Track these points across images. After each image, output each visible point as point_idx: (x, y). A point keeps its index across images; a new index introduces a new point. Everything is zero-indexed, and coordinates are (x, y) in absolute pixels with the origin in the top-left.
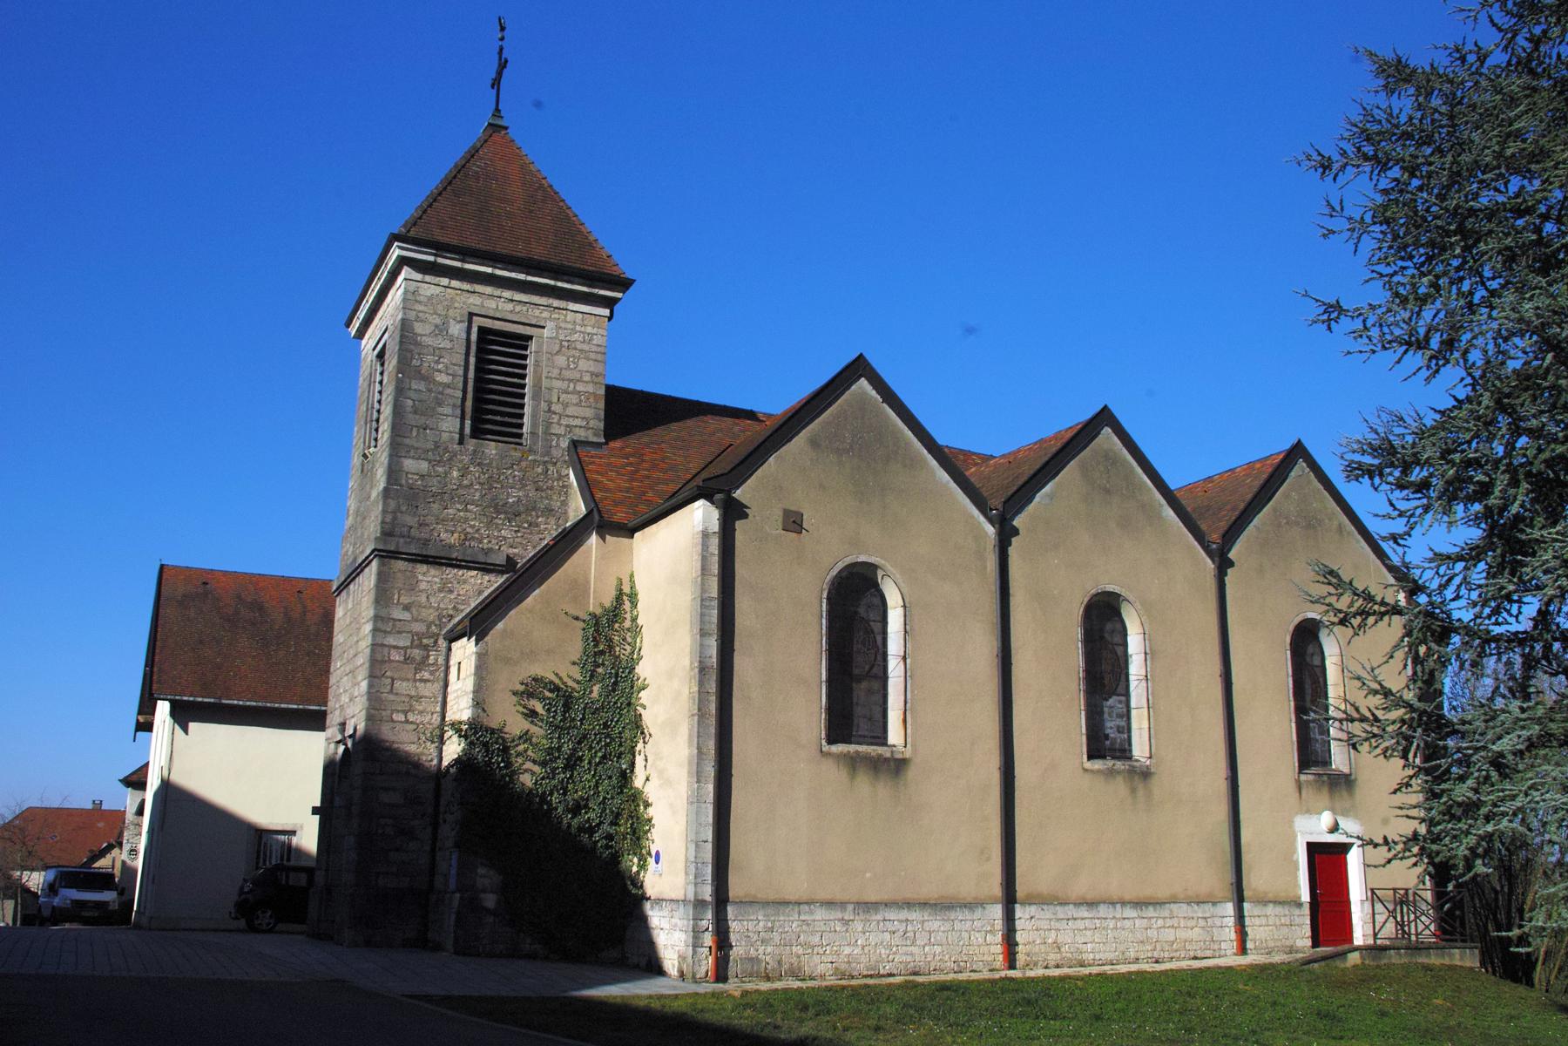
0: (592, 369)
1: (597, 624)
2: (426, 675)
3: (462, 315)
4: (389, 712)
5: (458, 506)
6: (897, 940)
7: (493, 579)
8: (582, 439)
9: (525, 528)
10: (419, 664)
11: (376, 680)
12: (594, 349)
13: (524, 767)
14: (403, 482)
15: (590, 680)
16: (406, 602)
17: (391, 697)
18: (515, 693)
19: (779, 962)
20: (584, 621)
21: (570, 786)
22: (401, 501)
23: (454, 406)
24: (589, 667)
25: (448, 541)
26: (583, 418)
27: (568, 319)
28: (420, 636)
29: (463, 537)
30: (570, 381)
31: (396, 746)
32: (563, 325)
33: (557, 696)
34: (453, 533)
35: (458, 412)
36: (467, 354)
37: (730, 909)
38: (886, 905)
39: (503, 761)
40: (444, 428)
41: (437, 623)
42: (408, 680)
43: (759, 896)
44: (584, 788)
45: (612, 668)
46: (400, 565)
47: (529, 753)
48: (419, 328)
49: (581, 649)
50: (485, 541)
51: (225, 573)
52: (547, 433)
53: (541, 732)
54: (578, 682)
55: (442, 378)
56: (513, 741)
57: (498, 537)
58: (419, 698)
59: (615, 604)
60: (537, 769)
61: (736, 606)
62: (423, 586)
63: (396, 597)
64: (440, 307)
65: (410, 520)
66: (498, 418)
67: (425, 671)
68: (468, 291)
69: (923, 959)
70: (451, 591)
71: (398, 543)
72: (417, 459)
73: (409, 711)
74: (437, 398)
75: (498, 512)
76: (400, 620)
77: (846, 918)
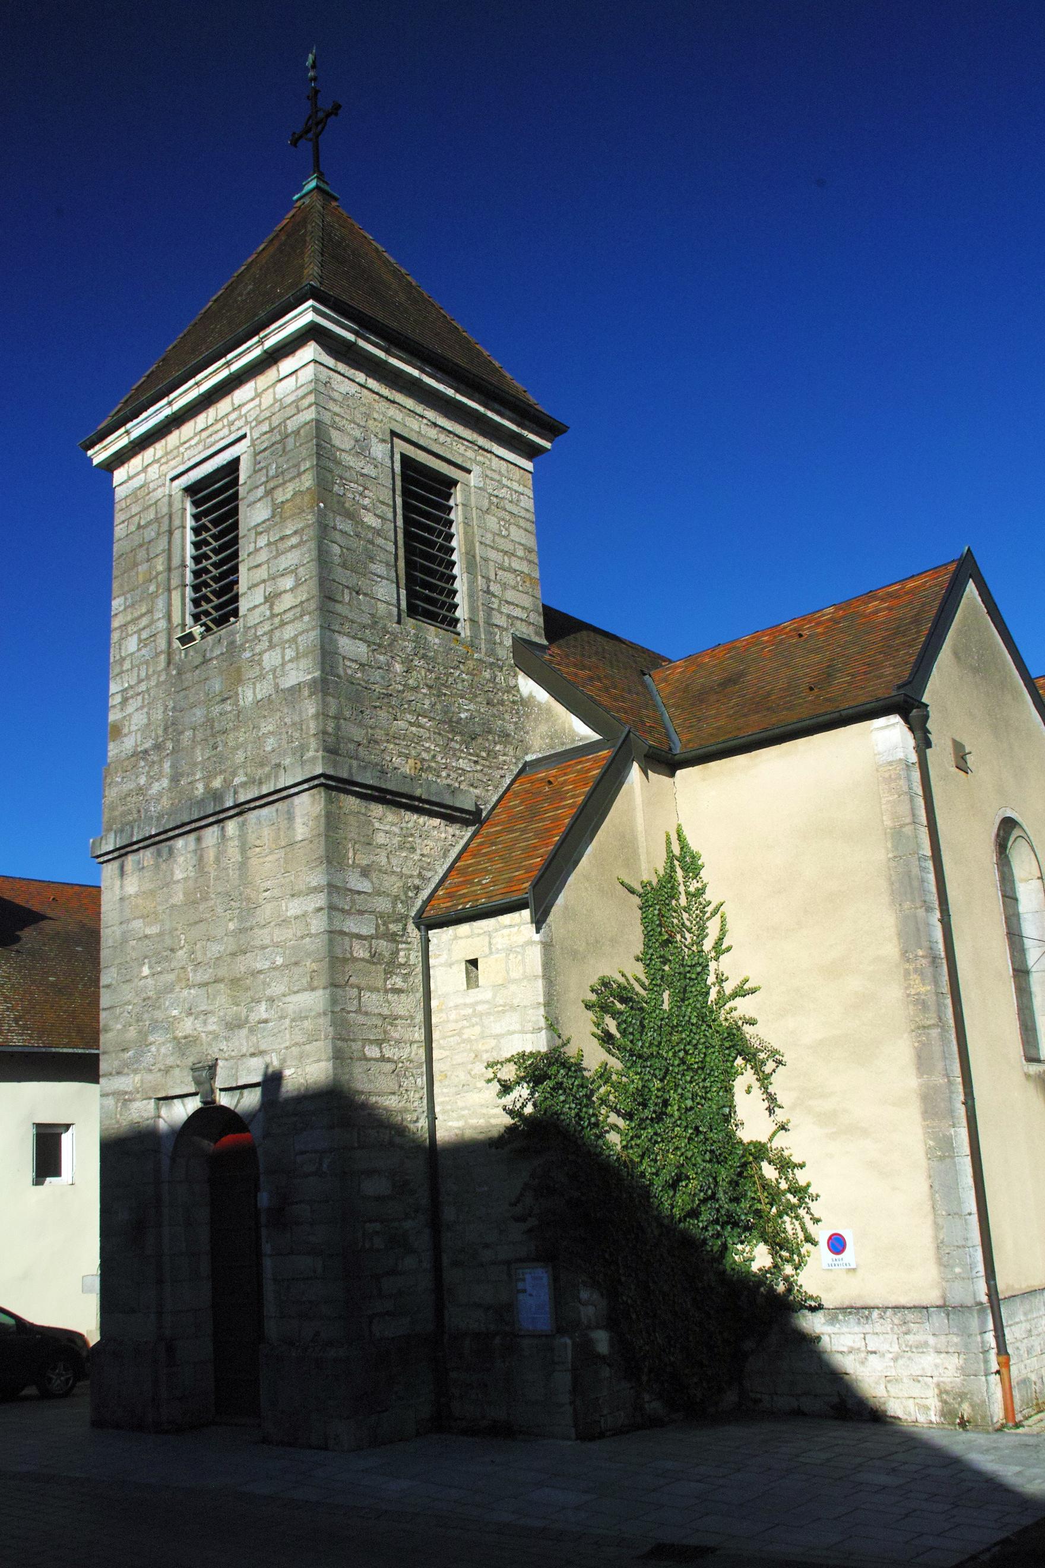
4: (360, 1043)
5: (409, 717)
7: (457, 832)
10: (388, 964)
11: (340, 991)
14: (341, 672)
16: (365, 862)
17: (361, 1019)
23: (388, 564)
26: (523, 608)
28: (384, 918)
29: (419, 766)
31: (373, 1099)
52: (489, 624)
63: (351, 854)
65: (358, 734)
68: (386, 398)
70: (413, 849)
71: (351, 767)
73: (384, 1041)
76: (359, 893)
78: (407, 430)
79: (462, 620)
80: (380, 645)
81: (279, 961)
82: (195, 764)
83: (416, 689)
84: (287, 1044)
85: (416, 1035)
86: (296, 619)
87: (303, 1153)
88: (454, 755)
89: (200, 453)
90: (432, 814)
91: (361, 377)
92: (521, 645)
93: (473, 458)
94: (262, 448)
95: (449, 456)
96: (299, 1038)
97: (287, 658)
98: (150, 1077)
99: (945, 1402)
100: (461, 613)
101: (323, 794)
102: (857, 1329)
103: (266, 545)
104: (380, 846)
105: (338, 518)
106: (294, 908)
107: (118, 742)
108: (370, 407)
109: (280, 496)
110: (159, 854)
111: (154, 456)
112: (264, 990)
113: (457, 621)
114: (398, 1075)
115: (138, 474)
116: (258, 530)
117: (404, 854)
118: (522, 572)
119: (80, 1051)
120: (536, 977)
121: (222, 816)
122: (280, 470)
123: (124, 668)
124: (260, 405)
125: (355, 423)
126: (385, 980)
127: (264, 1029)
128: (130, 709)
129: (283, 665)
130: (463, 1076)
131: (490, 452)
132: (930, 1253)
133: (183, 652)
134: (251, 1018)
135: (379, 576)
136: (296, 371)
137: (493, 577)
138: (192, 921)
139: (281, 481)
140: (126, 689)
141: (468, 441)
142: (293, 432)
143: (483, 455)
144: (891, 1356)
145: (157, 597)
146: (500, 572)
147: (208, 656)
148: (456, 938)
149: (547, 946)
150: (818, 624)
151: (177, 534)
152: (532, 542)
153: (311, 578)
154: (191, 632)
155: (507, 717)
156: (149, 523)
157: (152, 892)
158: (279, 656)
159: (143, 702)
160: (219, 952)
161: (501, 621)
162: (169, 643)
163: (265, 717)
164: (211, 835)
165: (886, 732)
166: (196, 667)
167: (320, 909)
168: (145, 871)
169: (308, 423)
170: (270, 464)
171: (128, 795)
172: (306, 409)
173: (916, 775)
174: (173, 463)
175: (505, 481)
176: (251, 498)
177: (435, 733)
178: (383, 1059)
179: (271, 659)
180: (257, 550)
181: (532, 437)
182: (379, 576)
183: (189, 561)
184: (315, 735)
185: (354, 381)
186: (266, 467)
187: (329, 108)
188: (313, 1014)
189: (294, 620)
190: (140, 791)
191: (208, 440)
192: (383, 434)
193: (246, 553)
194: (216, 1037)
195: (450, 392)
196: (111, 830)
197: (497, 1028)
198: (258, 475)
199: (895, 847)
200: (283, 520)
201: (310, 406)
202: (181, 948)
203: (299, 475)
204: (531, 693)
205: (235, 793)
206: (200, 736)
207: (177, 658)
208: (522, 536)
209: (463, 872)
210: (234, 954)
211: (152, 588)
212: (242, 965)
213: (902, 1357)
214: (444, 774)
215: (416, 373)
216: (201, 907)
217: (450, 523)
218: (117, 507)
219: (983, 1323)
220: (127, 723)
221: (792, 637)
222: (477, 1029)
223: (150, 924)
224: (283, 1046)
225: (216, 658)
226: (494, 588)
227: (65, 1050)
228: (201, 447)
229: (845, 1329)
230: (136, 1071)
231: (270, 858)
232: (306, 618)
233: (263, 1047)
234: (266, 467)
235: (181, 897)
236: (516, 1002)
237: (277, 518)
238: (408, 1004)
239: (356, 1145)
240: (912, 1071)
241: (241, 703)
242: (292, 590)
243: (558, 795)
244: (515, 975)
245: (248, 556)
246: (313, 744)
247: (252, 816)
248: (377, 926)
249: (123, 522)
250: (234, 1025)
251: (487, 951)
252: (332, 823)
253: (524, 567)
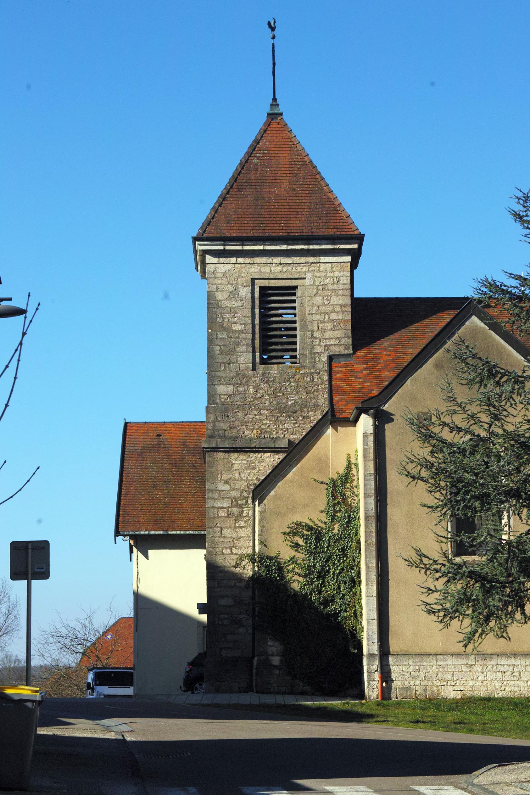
0: (341, 302)
1: (334, 486)
2: (242, 524)
3: (247, 282)
4: (220, 549)
5: (255, 412)
6: (507, 677)
8: (337, 353)
9: (300, 420)
12: (341, 287)
13: (293, 578)
14: (218, 401)
15: (332, 522)
16: (226, 478)
17: (221, 539)
18: (285, 534)
19: (425, 690)
20: (327, 484)
21: (323, 589)
22: (217, 414)
23: (247, 345)
24: (330, 513)
25: (250, 436)
27: (321, 269)
29: (259, 432)
30: (326, 313)
31: (227, 569)
32: (318, 274)
33: (311, 534)
34: (252, 430)
35: (250, 348)
36: (253, 308)
37: (391, 659)
38: (498, 655)
39: (278, 576)
40: (242, 361)
41: (247, 489)
42: (231, 528)
43: (410, 650)
44: (331, 590)
45: (346, 513)
46: (220, 455)
47: (296, 570)
48: (219, 296)
49: (326, 502)
50: (274, 433)
51: (175, 424)
53: (303, 556)
54: (325, 523)
55: (237, 327)
56: (285, 563)
57: (282, 429)
58: (238, 539)
59: (346, 471)
60: (301, 579)
61: (388, 476)
62: (236, 467)
63: (219, 476)
64: (232, 279)
66: (279, 347)
67: (242, 521)
68: (249, 263)
69: (526, 689)
71: (217, 442)
72: (226, 384)
74: (235, 342)
75: (281, 412)
76: (223, 491)
77: (469, 663)
135: (242, 352)
239: (216, 586)
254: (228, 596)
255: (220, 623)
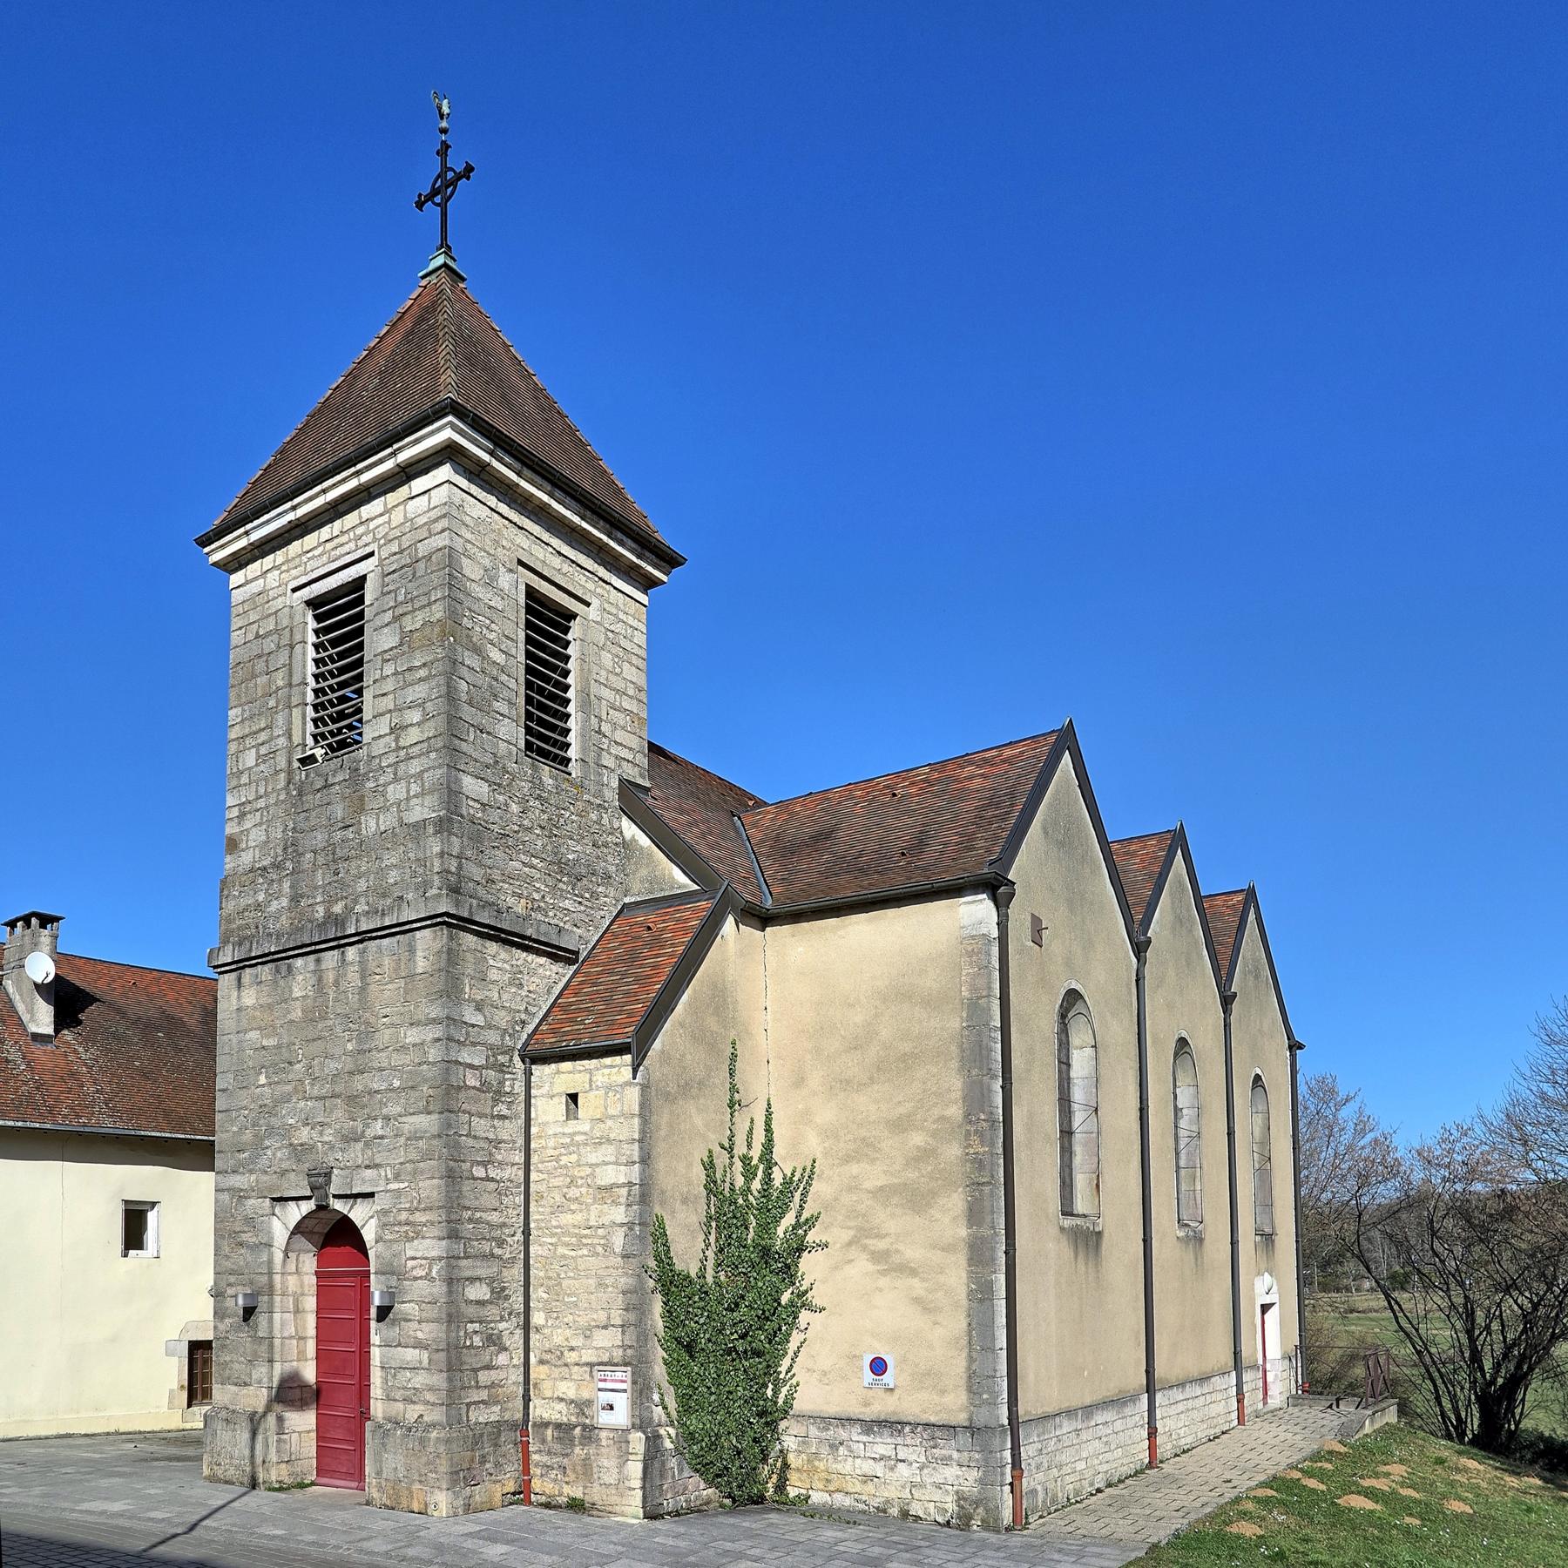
7: (561, 970)
14: (465, 813)
17: (471, 1142)
26: (630, 749)
29: (530, 906)
63: (467, 990)
65: (476, 873)
68: (515, 524)
71: (471, 906)
76: (473, 1026)
78: (533, 558)
79: (573, 760)
80: (499, 785)
81: (396, 1083)
82: (316, 888)
83: (529, 829)
84: (402, 1160)
85: (517, 1158)
86: (422, 754)
87: (414, 1258)
88: (561, 896)
89: (324, 565)
90: (538, 953)
91: (492, 501)
92: (628, 789)
93: (593, 589)
94: (391, 570)
95: (571, 588)
96: (413, 1156)
97: (412, 793)
98: (265, 1178)
99: (962, 1507)
100: (572, 753)
101: (445, 932)
102: (889, 1441)
103: (394, 674)
104: (494, 982)
105: (467, 653)
106: (412, 1036)
107: (235, 856)
108: (500, 533)
109: (409, 624)
110: (278, 971)
111: (275, 561)
112: (381, 1109)
113: (569, 760)
114: (499, 1194)
115: (256, 579)
116: (385, 657)
117: (513, 990)
118: (632, 712)
119: (168, 1135)
120: (633, 1115)
121: (343, 942)
122: (409, 596)
123: (242, 782)
124: (389, 522)
125: (485, 551)
126: (492, 1107)
127: (380, 1144)
128: (248, 825)
129: (408, 799)
130: (559, 1199)
131: (609, 584)
132: (963, 1382)
133: (304, 773)
134: (367, 1134)
135: (502, 715)
136: (429, 490)
137: (604, 718)
138: (310, 1038)
139: (410, 609)
140: (243, 803)
141: (589, 571)
142: (424, 557)
143: (602, 587)
144: (918, 1465)
145: (276, 713)
146: (611, 712)
147: (331, 780)
148: (558, 1072)
149: (645, 1088)
150: (913, 784)
151: (298, 648)
152: (642, 680)
153: (439, 714)
154: (313, 754)
155: (610, 858)
156: (268, 634)
157: (270, 1007)
158: (404, 790)
159: (261, 819)
160: (337, 1069)
161: (608, 761)
162: (290, 763)
163: (388, 849)
164: (330, 959)
165: (973, 906)
166: (318, 790)
167: (438, 1040)
168: (262, 985)
169: (441, 549)
170: (398, 588)
171: (245, 910)
172: (438, 533)
173: (995, 950)
174: (294, 572)
175: (622, 616)
176: (378, 622)
177: (545, 874)
178: (488, 1179)
179: (395, 792)
180: (384, 678)
181: (650, 569)
182: (502, 715)
183: (311, 681)
184: (438, 873)
185: (485, 504)
186: (395, 591)
187: (460, 169)
188: (428, 1135)
189: (420, 755)
190: (258, 906)
191: (333, 553)
192: (511, 562)
193: (372, 679)
194: (332, 1148)
195: (576, 519)
196: (229, 942)
197: (593, 1158)
198: (386, 598)
199: (970, 1018)
200: (412, 649)
201: (443, 531)
202: (299, 1062)
203: (429, 604)
204: (633, 836)
205: (357, 921)
206: (321, 860)
207: (298, 778)
208: (634, 675)
209: (565, 1009)
210: (351, 1073)
211: (272, 703)
212: (359, 1084)
213: (928, 1467)
214: (551, 914)
215: (545, 498)
216: (320, 1026)
217: (567, 658)
218: (234, 611)
219: (1004, 1442)
220: (245, 838)
221: (884, 794)
222: (574, 1158)
223: (268, 1036)
224: (397, 1161)
225: (339, 783)
226: (605, 728)
227: (153, 1134)
228: (325, 559)
229: (878, 1440)
230: (251, 1172)
231: (390, 986)
232: (433, 755)
233: (377, 1161)
234: (395, 591)
235: (300, 1014)
236: (612, 1136)
237: (405, 648)
238: (511, 1130)
239: (462, 1255)
240: (963, 1222)
241: (364, 832)
242: (418, 724)
243: (657, 942)
244: (611, 1111)
245: (374, 682)
246: (437, 881)
247: (372, 944)
248: (488, 1057)
249: (240, 628)
250: (350, 1138)
251: (587, 1086)
252: (451, 958)
253: (631, 706)
254: (479, 1279)
255: (468, 1343)
